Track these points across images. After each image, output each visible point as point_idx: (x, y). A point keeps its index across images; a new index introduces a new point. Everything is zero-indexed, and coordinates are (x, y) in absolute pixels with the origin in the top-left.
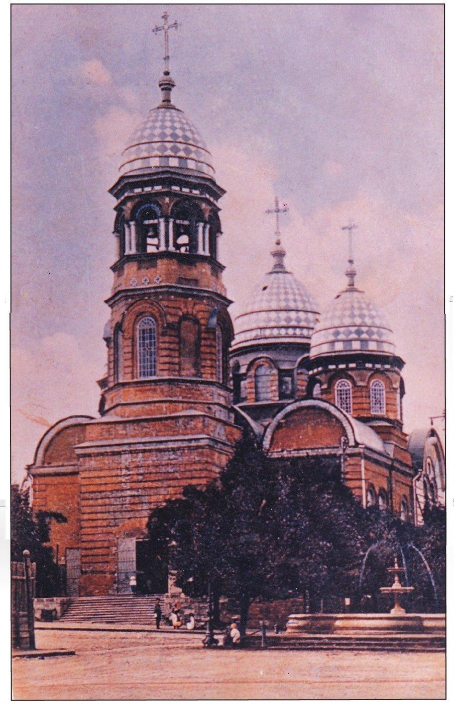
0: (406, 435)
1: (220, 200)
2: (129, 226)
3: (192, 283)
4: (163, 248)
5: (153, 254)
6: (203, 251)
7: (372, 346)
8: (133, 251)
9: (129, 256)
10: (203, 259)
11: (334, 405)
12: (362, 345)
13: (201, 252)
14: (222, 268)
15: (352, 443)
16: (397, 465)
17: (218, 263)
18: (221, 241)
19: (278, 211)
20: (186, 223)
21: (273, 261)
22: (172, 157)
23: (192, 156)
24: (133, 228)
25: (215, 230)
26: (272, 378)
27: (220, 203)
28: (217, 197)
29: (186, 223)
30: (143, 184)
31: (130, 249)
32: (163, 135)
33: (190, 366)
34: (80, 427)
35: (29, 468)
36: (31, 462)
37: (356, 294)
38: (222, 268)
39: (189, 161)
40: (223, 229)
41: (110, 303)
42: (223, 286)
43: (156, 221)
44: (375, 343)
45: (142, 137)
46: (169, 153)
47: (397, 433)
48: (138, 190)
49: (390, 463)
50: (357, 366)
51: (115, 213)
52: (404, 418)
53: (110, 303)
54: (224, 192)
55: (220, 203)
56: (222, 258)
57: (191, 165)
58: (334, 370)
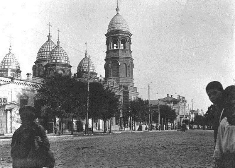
1: (131, 36)
2: (110, 44)
5: (115, 50)
7: (58, 61)
9: (110, 50)
10: (127, 50)
12: (55, 61)
14: (132, 52)
18: (131, 46)
25: (130, 43)
26: (18, 118)
27: (131, 37)
28: (131, 36)
33: (116, 94)
38: (132, 52)
41: (167, 129)
42: (132, 56)
44: (59, 61)
51: (106, 40)
53: (167, 129)
54: (132, 35)
55: (131, 37)
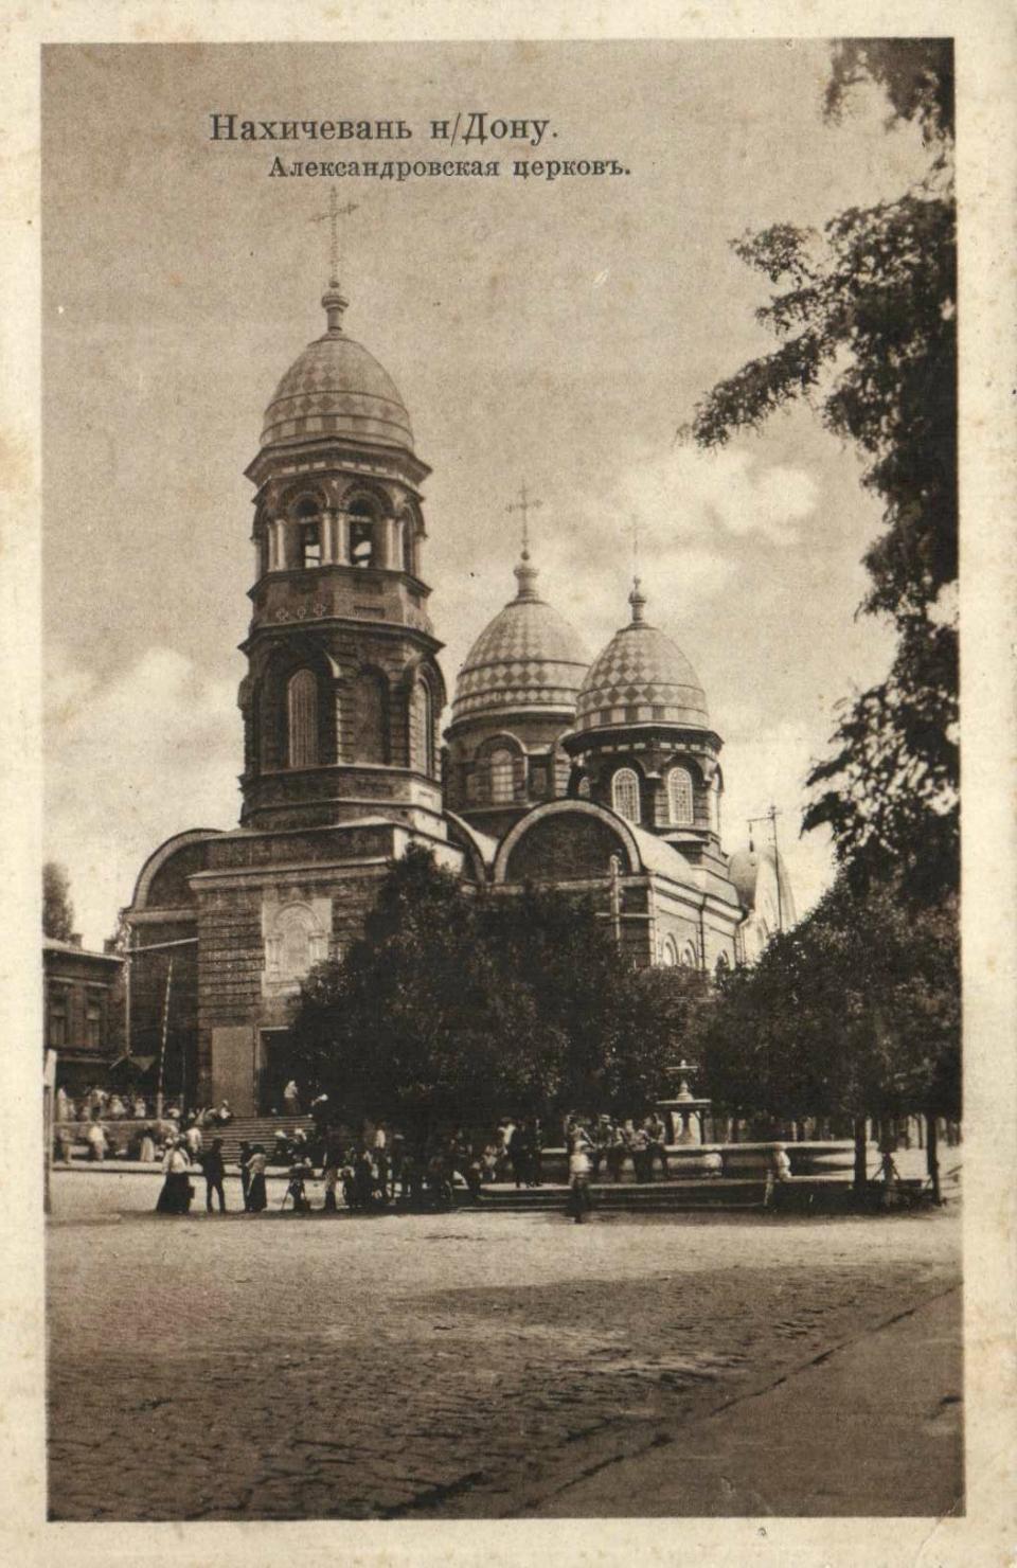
6: (394, 562)
13: (391, 566)
20: (366, 520)
24: (280, 529)
29: (366, 520)
43: (316, 518)
46: (337, 409)
49: (698, 899)
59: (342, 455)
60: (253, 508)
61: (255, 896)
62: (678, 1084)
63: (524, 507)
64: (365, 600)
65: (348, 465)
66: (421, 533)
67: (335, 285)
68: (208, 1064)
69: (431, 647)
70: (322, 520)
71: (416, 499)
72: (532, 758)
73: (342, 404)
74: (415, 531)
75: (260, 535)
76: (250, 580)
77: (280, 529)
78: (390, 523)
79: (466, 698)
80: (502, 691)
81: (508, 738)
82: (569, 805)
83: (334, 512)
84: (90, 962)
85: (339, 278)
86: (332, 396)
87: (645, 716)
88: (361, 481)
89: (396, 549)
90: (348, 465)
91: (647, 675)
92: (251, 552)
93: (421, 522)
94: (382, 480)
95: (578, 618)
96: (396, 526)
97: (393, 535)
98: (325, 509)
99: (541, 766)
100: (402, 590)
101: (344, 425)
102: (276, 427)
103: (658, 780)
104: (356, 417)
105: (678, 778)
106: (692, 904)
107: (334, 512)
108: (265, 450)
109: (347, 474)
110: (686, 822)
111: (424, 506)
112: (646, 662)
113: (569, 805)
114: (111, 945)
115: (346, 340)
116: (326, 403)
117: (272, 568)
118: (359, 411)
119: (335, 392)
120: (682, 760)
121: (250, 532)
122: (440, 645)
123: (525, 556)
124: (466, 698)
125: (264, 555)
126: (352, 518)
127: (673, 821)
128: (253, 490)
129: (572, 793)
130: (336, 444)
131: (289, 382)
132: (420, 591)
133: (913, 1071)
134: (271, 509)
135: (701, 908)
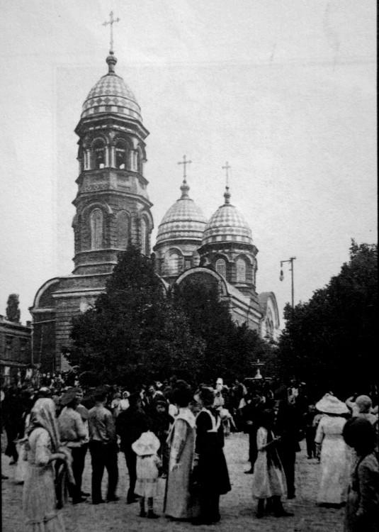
0: (257, 294)
3: (13, 378)
4: (107, 166)
6: (134, 168)
8: (89, 168)
11: (215, 271)
13: (132, 170)
15: (225, 294)
16: (252, 310)
17: (143, 178)
19: (185, 163)
20: (122, 151)
21: (180, 193)
22: (113, 106)
23: (127, 106)
24: (89, 154)
29: (122, 151)
30: (96, 124)
31: (87, 167)
32: (101, 92)
34: (58, 283)
35: (30, 309)
36: (31, 305)
37: (230, 208)
39: (125, 109)
40: (148, 157)
43: (103, 149)
45: (94, 93)
46: (111, 103)
47: (252, 291)
48: (123, 128)
49: (247, 309)
50: (356, 515)
52: (256, 283)
56: (147, 173)
57: (126, 111)
58: (215, 253)
59: (114, 122)
60: (78, 146)
61: (78, 300)
62: (256, 369)
63: (185, 163)
64: (121, 183)
65: (116, 126)
66: (145, 159)
67: (111, 53)
68: (60, 365)
69: (148, 205)
70: (105, 149)
71: (143, 145)
72: (185, 257)
73: (114, 100)
74: (142, 159)
75: (81, 157)
76: (77, 174)
77: (89, 154)
78: (132, 152)
79: (161, 234)
80: (175, 232)
81: (177, 249)
82: (200, 269)
83: (110, 146)
84: (21, 329)
85: (114, 50)
86: (110, 97)
87: (229, 239)
88: (122, 134)
89: (134, 159)
90: (116, 126)
91: (230, 223)
92: (77, 164)
93: (144, 152)
94: (129, 133)
95: (204, 208)
96: (134, 154)
97: (133, 159)
98: (106, 145)
99: (189, 260)
100: (137, 180)
101: (114, 109)
102: (87, 110)
103: (233, 263)
104: (119, 107)
105: (241, 263)
106: (244, 310)
107: (110, 146)
108: (82, 120)
109: (115, 130)
110: (244, 279)
111: (146, 149)
112: (230, 218)
113: (200, 269)
114: (28, 323)
115: (116, 76)
116: (107, 100)
117: (86, 169)
118: (120, 104)
119: (111, 96)
120: (243, 256)
121: (76, 155)
122: (152, 205)
123: (185, 182)
124: (161, 234)
125: (82, 166)
126: (117, 150)
127: (238, 280)
128: (77, 138)
129: (201, 265)
130: (111, 117)
131: (91, 98)
132: (144, 182)
133: (142, 398)
134: (84, 145)
135: (248, 312)
